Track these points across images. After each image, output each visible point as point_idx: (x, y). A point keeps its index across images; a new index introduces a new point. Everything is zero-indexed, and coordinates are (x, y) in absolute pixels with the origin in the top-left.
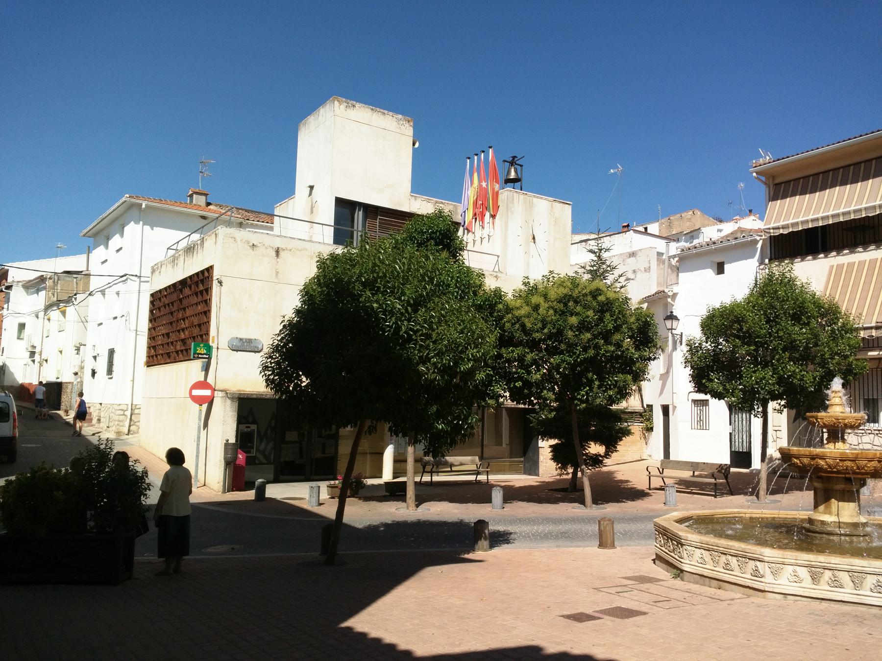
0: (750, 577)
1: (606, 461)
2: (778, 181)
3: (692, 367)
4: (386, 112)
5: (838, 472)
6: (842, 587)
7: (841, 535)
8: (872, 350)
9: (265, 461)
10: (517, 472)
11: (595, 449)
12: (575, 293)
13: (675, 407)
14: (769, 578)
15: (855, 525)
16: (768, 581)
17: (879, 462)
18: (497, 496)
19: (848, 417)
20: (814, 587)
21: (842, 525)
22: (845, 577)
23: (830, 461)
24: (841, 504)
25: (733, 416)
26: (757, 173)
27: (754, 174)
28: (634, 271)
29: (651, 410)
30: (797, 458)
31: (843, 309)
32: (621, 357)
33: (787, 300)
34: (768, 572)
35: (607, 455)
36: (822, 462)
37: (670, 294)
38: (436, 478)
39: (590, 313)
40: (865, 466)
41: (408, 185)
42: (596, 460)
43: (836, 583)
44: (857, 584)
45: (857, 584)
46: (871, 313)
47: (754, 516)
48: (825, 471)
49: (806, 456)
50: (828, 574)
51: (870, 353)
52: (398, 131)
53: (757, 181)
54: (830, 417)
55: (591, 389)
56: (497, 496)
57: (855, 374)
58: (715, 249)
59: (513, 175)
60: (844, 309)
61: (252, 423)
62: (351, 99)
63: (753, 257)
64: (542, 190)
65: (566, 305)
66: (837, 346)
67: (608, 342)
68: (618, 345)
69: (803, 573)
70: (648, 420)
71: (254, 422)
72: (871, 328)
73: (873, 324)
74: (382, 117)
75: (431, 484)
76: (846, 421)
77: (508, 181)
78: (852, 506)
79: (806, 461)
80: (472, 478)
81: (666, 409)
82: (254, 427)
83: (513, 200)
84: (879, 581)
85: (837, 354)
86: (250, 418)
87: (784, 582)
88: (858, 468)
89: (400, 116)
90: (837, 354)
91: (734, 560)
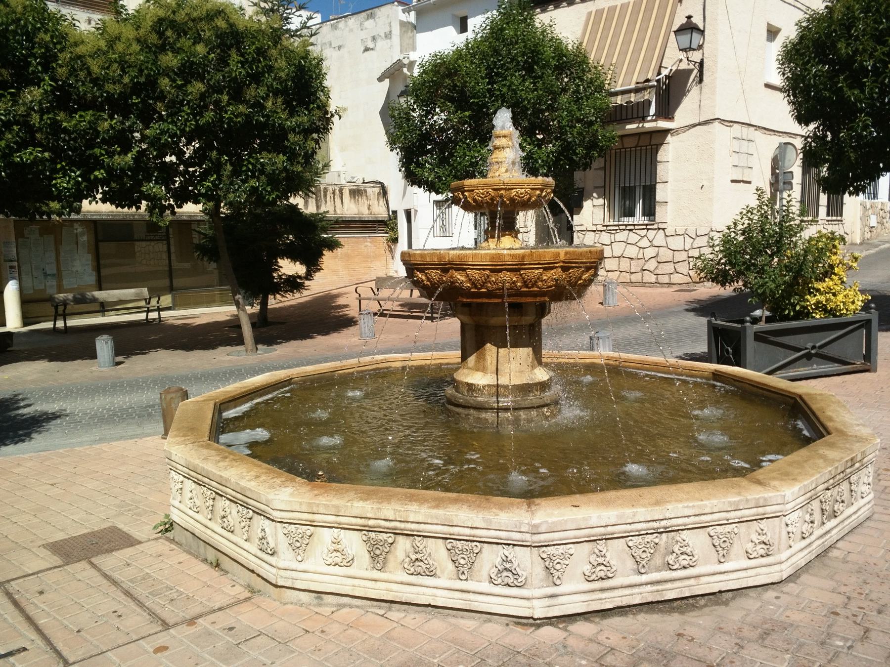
0: (254, 549)
1: (307, 283)
3: (401, 149)
5: (490, 294)
6: (432, 574)
7: (499, 409)
8: (630, 123)
9: (592, 271)
10: (209, 302)
11: (288, 267)
12: (181, 17)
13: (416, 211)
14: (286, 558)
15: (525, 389)
16: (284, 564)
17: (565, 269)
18: (104, 346)
19: (520, 185)
20: (376, 574)
21: (501, 390)
22: (438, 552)
23: (475, 274)
25: (478, 217)
28: (374, 38)
29: (396, 218)
30: (422, 271)
31: (592, 57)
32: (265, 126)
33: (517, 43)
34: (282, 545)
35: (309, 276)
36: (460, 277)
37: (406, 61)
38: (73, 322)
39: (201, 49)
40: (539, 279)
42: (294, 284)
43: (420, 567)
44: (463, 568)
45: (463, 568)
46: (630, 72)
48: (467, 293)
50: (403, 544)
51: (628, 127)
54: (486, 185)
55: (219, 178)
57: (601, 149)
60: (592, 57)
65: (161, 34)
66: (579, 110)
67: (237, 96)
68: (258, 106)
69: (354, 543)
70: (392, 229)
72: (629, 91)
73: (633, 86)
75: (67, 330)
76: (513, 193)
78: (525, 353)
79: (435, 274)
80: (142, 316)
81: (408, 213)
84: (506, 560)
85: (579, 121)
87: (316, 568)
88: (474, 285)
90: (579, 121)
91: (234, 508)
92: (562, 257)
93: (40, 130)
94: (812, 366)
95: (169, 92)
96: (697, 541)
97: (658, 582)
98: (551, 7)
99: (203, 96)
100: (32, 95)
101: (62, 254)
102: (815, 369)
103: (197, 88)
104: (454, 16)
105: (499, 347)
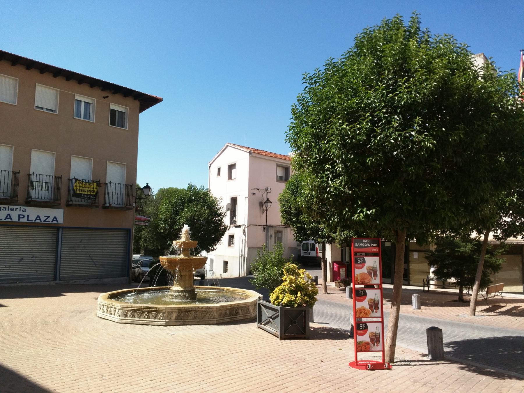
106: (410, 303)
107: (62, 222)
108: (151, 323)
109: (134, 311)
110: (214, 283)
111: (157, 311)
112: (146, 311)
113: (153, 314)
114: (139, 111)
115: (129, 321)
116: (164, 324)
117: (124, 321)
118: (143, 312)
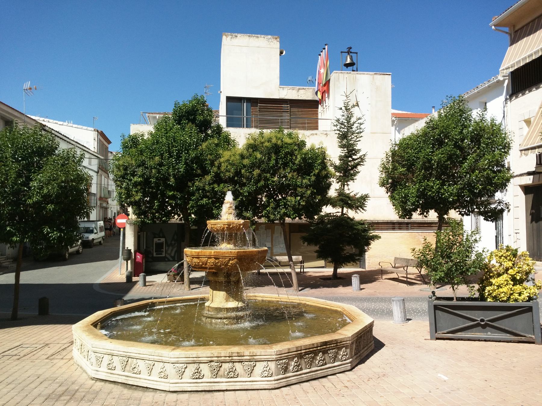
2: (517, 28)
4: (259, 36)
9: (171, 259)
17: (216, 259)
18: (355, 280)
24: (214, 292)
26: (495, 26)
27: (493, 27)
41: (278, 81)
47: (265, 299)
49: (206, 256)
52: (269, 46)
53: (497, 31)
56: (355, 280)
58: (478, 92)
59: (349, 61)
61: (162, 237)
62: (234, 33)
63: (502, 95)
64: (368, 69)
71: (163, 237)
74: (257, 39)
77: (347, 65)
82: (163, 240)
83: (339, 79)
86: (161, 235)
89: (270, 37)
92: (213, 254)
93: (208, 192)
94: (487, 332)
95: (193, 184)
96: (142, 366)
97: (127, 376)
98: (527, 92)
99: (259, 175)
100: (208, 178)
101: (274, 238)
102: (489, 334)
103: (256, 172)
104: (480, 103)
105: (213, 290)
106: (389, 313)
107: (209, 227)
108: (330, 371)
109: (300, 356)
110: (145, 279)
111: (337, 345)
112: (320, 351)
113: (331, 353)
114: (509, 44)
115: (293, 380)
116: (349, 368)
117: (283, 382)
118: (316, 353)
